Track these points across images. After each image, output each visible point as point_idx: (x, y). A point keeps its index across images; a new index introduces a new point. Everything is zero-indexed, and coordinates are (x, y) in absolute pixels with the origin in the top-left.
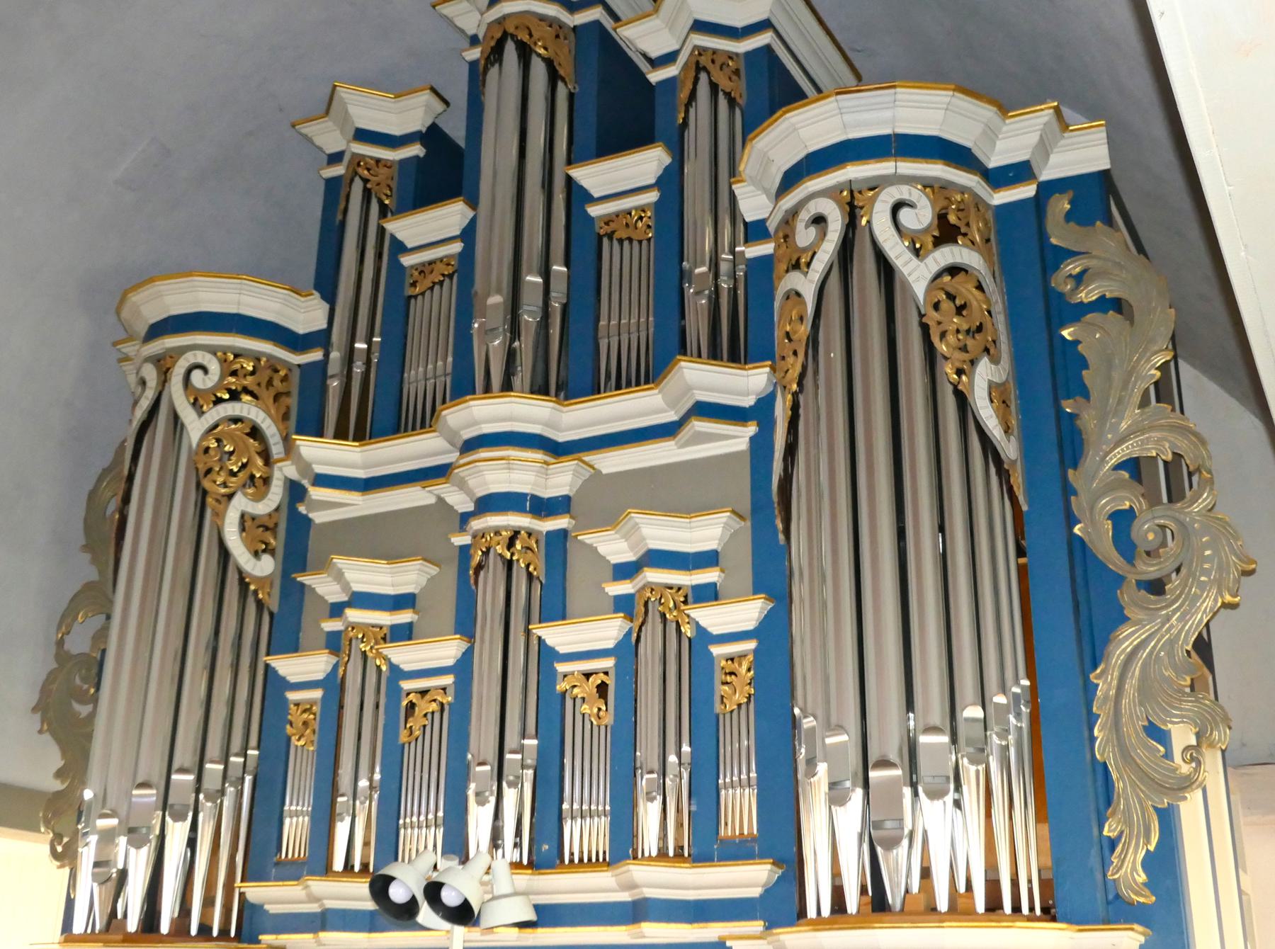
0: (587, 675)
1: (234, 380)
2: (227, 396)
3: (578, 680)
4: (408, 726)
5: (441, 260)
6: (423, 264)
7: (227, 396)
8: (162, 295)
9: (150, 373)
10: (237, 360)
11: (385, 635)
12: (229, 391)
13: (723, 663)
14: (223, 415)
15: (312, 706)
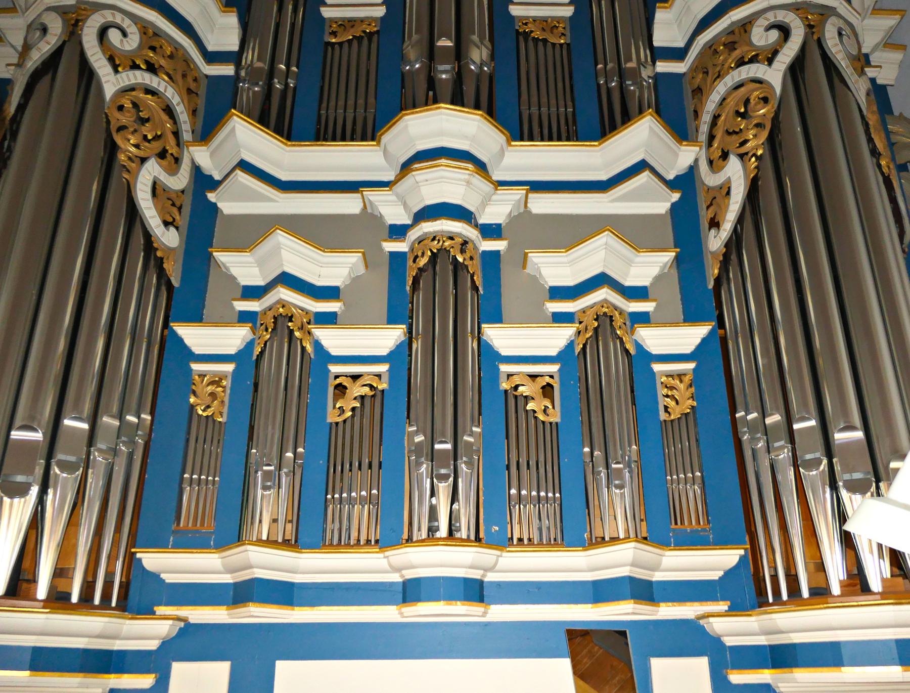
0: (533, 377)
4: (338, 405)
6: (343, 19)
10: (157, 38)
13: (664, 379)
15: (221, 379)
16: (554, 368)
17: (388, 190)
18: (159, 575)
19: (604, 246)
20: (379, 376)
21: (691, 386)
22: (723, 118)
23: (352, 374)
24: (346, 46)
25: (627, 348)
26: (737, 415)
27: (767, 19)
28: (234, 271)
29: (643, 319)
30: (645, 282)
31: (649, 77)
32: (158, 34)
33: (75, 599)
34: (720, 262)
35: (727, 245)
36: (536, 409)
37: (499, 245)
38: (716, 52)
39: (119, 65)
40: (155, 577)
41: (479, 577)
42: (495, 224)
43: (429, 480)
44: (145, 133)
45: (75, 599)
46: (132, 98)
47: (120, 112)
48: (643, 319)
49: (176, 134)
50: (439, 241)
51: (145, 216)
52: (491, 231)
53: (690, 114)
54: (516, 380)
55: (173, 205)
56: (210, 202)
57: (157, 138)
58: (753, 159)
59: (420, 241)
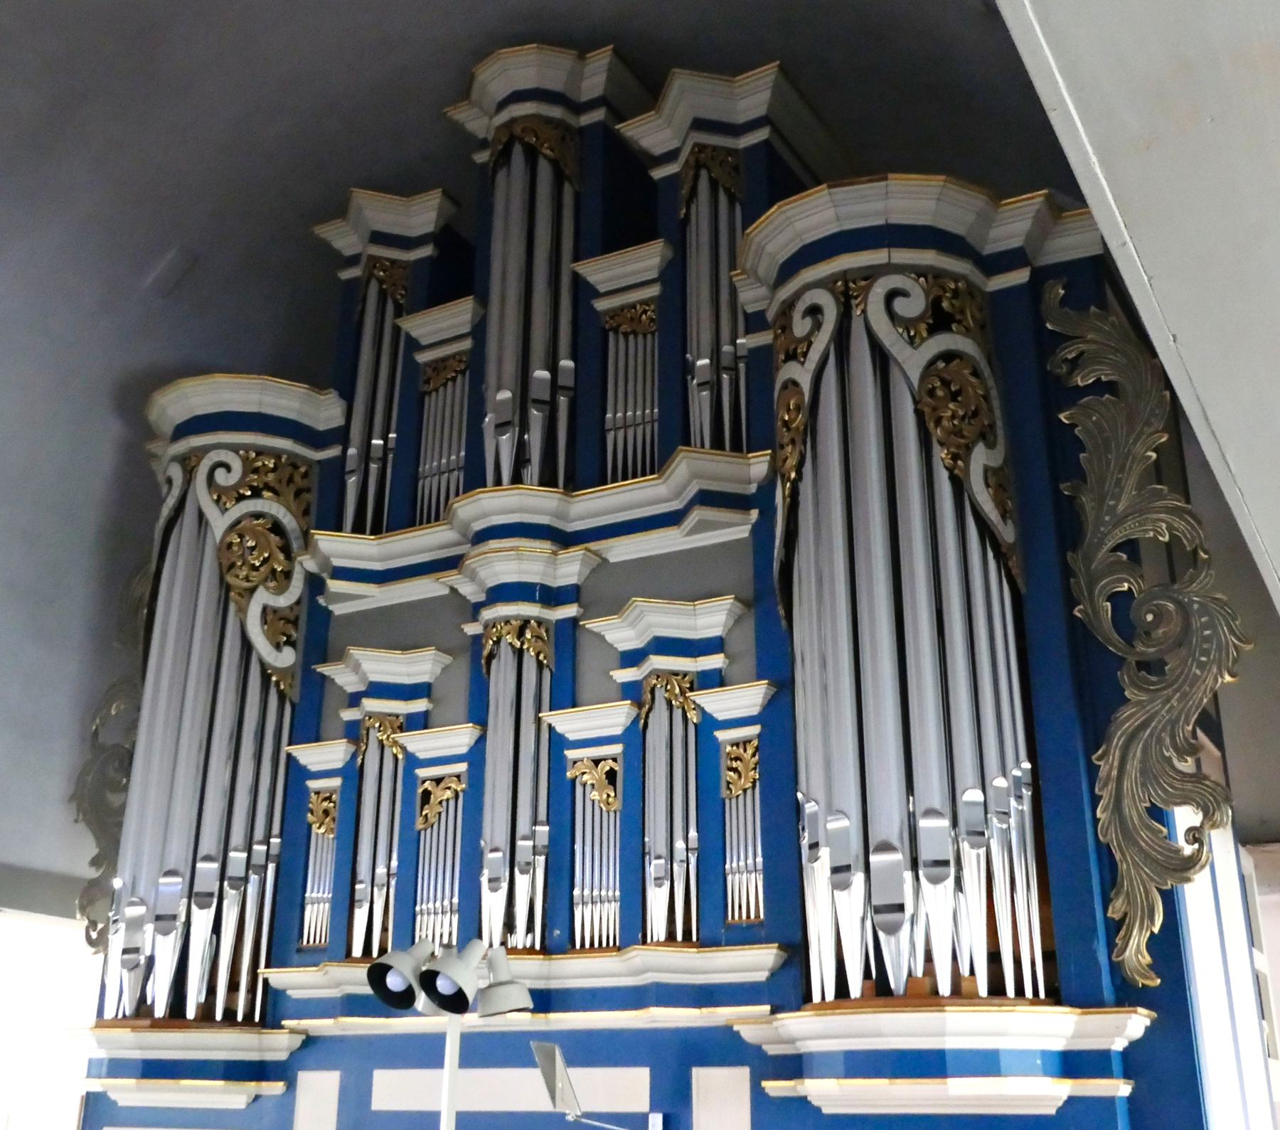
0: (597, 762)
4: (424, 813)
7: (249, 493)
12: (252, 488)
13: (729, 749)
16: (617, 749)
20: (458, 777)
30: (717, 632)
33: (240, 1018)
45: (240, 1018)
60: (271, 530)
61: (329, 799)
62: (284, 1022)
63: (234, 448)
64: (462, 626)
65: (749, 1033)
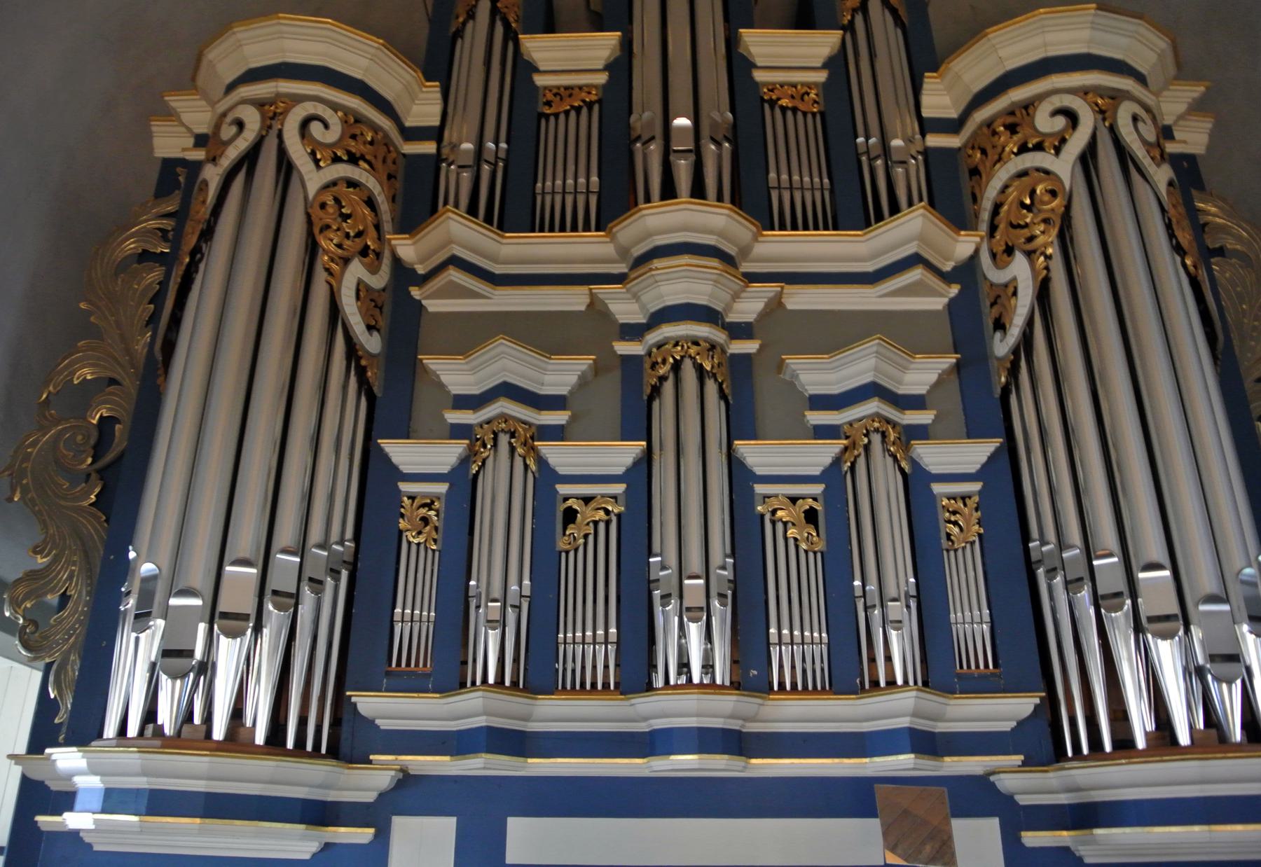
0: (794, 500)
1: (353, 144)
2: (345, 158)
3: (782, 503)
4: (568, 533)
5: (580, 88)
7: (345, 158)
8: (241, 45)
9: (252, 119)
10: (358, 125)
11: (533, 433)
12: (349, 153)
13: (945, 502)
14: (342, 175)
15: (433, 502)
16: (818, 489)
17: (624, 293)
18: (374, 721)
19: (874, 355)
20: (615, 497)
21: (977, 510)
22: (1005, 208)
23: (583, 496)
24: (562, 117)
25: (902, 466)
26: (1031, 545)
27: (1052, 103)
28: (445, 379)
29: (920, 432)
30: (922, 390)
31: (919, 152)
32: (359, 120)
34: (1008, 370)
35: (1015, 351)
36: (799, 537)
37: (749, 347)
38: (995, 133)
39: (320, 160)
40: (370, 723)
41: (737, 728)
42: (744, 323)
43: (676, 619)
44: (348, 230)
46: (334, 194)
47: (323, 210)
48: (920, 432)
49: (378, 227)
50: (683, 346)
51: (350, 323)
52: (740, 331)
53: (967, 198)
54: (775, 503)
55: (376, 306)
56: (414, 299)
57: (359, 234)
58: (1042, 259)
59: (659, 346)
60: (366, 202)
61: (429, 506)
62: (372, 757)
63: (335, 107)
64: (614, 344)
65: (1006, 783)
